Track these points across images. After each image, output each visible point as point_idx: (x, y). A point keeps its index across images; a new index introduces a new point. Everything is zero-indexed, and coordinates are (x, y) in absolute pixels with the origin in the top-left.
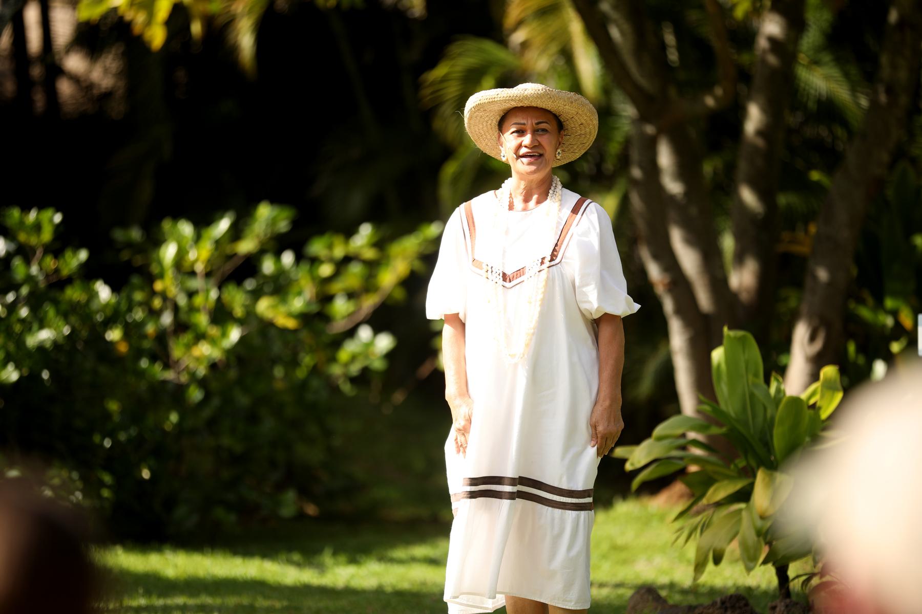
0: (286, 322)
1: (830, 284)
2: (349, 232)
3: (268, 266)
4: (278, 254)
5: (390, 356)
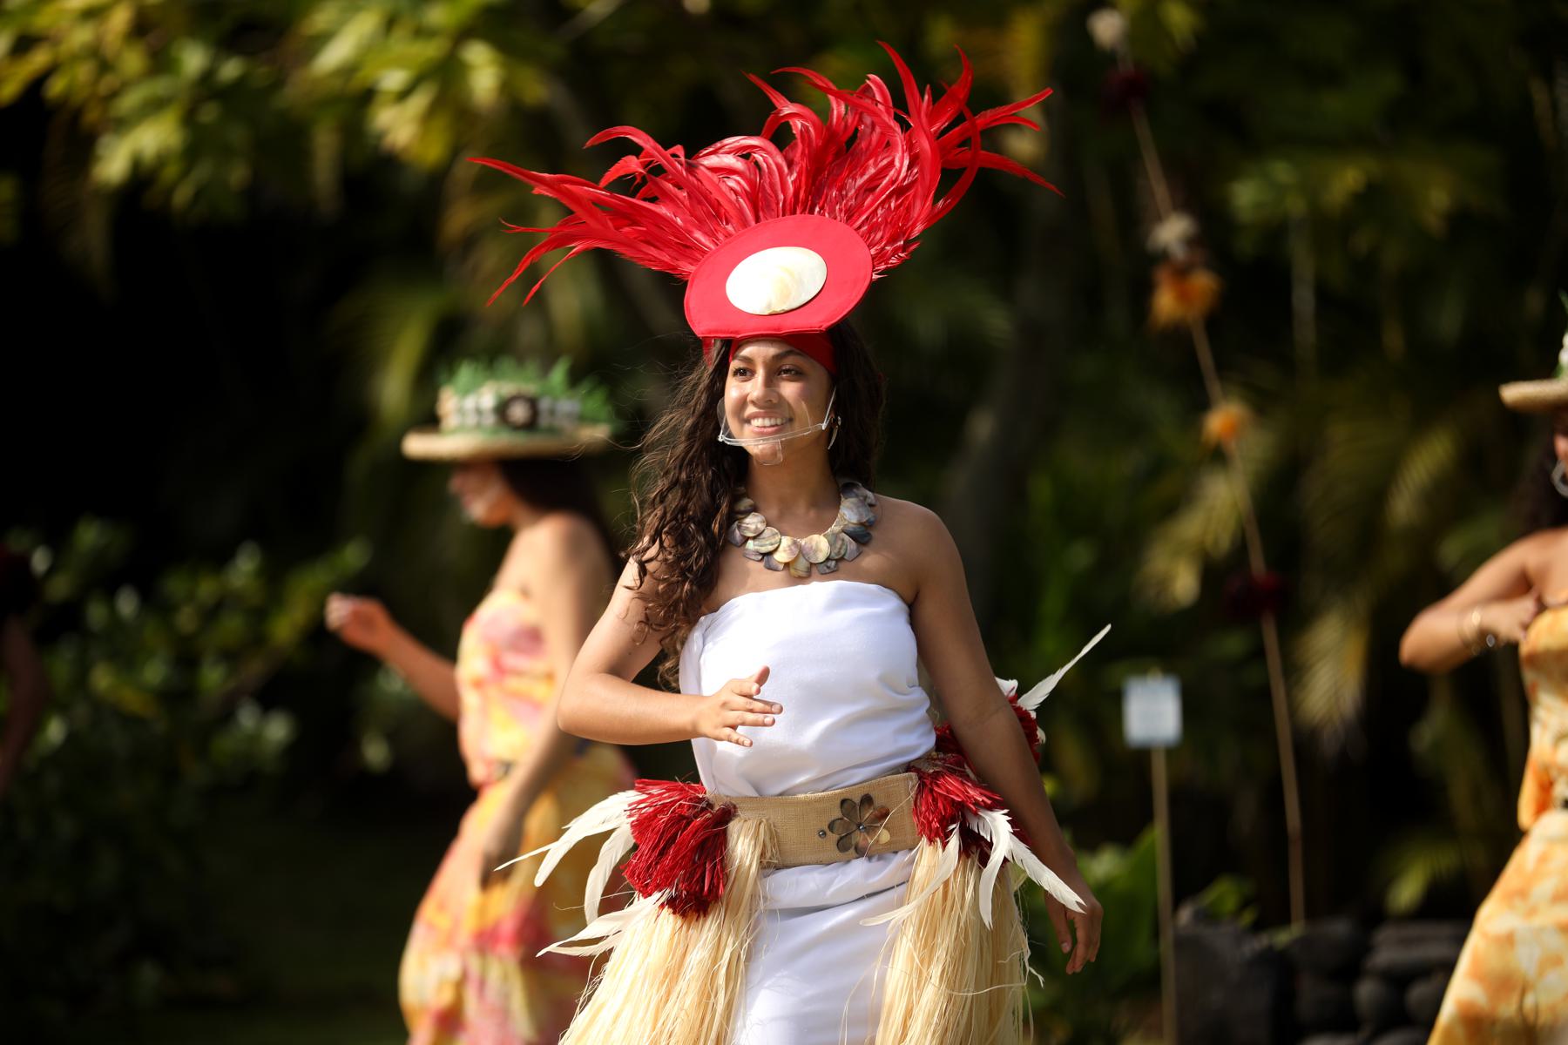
0: (133, 700)
1: (805, 396)
2: (221, 558)
3: (96, 614)
4: (110, 593)
5: (293, 750)
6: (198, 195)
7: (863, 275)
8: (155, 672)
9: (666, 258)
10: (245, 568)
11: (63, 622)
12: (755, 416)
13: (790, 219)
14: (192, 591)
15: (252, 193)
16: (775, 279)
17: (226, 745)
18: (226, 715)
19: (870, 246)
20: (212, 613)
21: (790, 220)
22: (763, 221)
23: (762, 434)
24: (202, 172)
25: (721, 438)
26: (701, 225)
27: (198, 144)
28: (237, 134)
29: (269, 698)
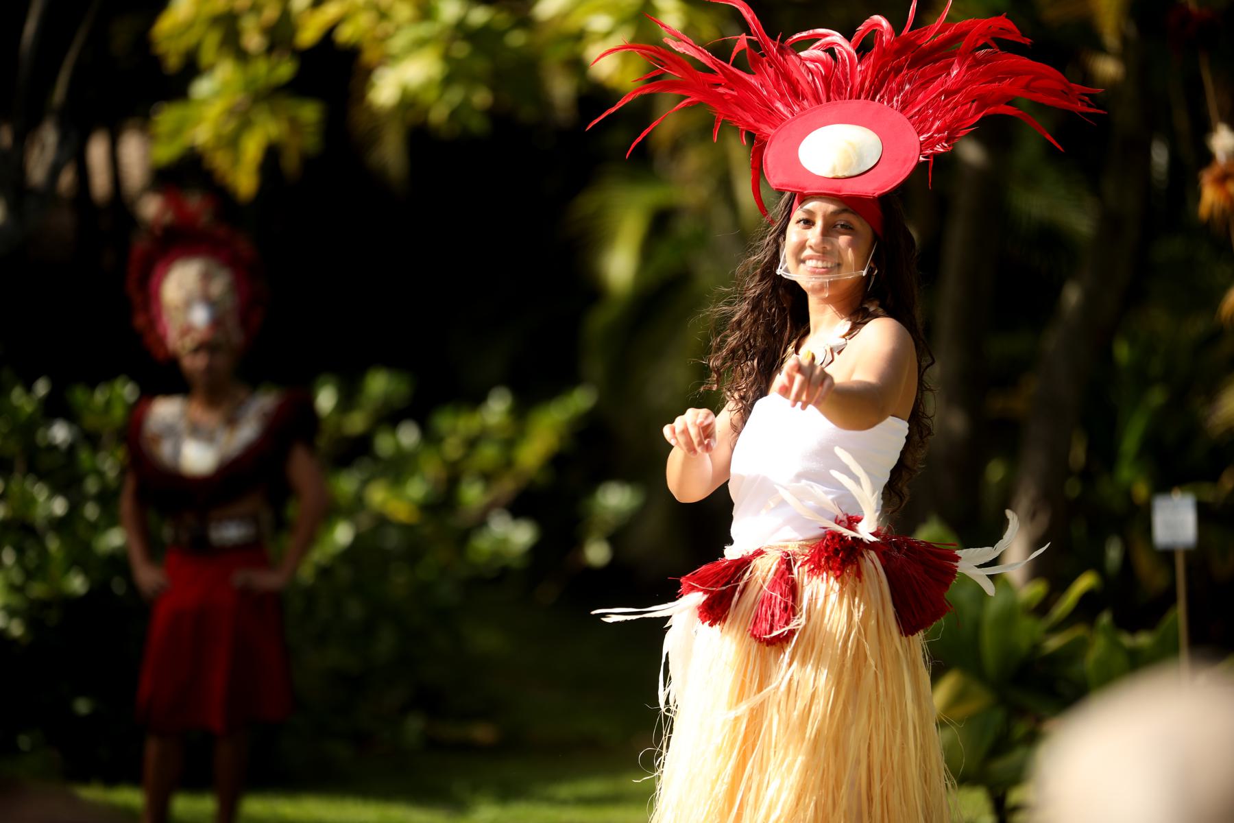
2: (476, 399)
3: (384, 444)
5: (535, 551)
6: (454, 114)
7: (911, 150)
8: (417, 489)
9: (751, 120)
10: (497, 408)
11: (355, 451)
12: (811, 258)
13: (854, 102)
14: (456, 426)
15: (495, 115)
16: (839, 148)
17: (483, 544)
18: (481, 523)
19: (919, 134)
20: (473, 443)
21: (855, 104)
22: (833, 101)
23: (814, 273)
24: (456, 95)
25: (779, 272)
26: (782, 98)
27: (453, 75)
28: (481, 65)
29: (519, 507)
